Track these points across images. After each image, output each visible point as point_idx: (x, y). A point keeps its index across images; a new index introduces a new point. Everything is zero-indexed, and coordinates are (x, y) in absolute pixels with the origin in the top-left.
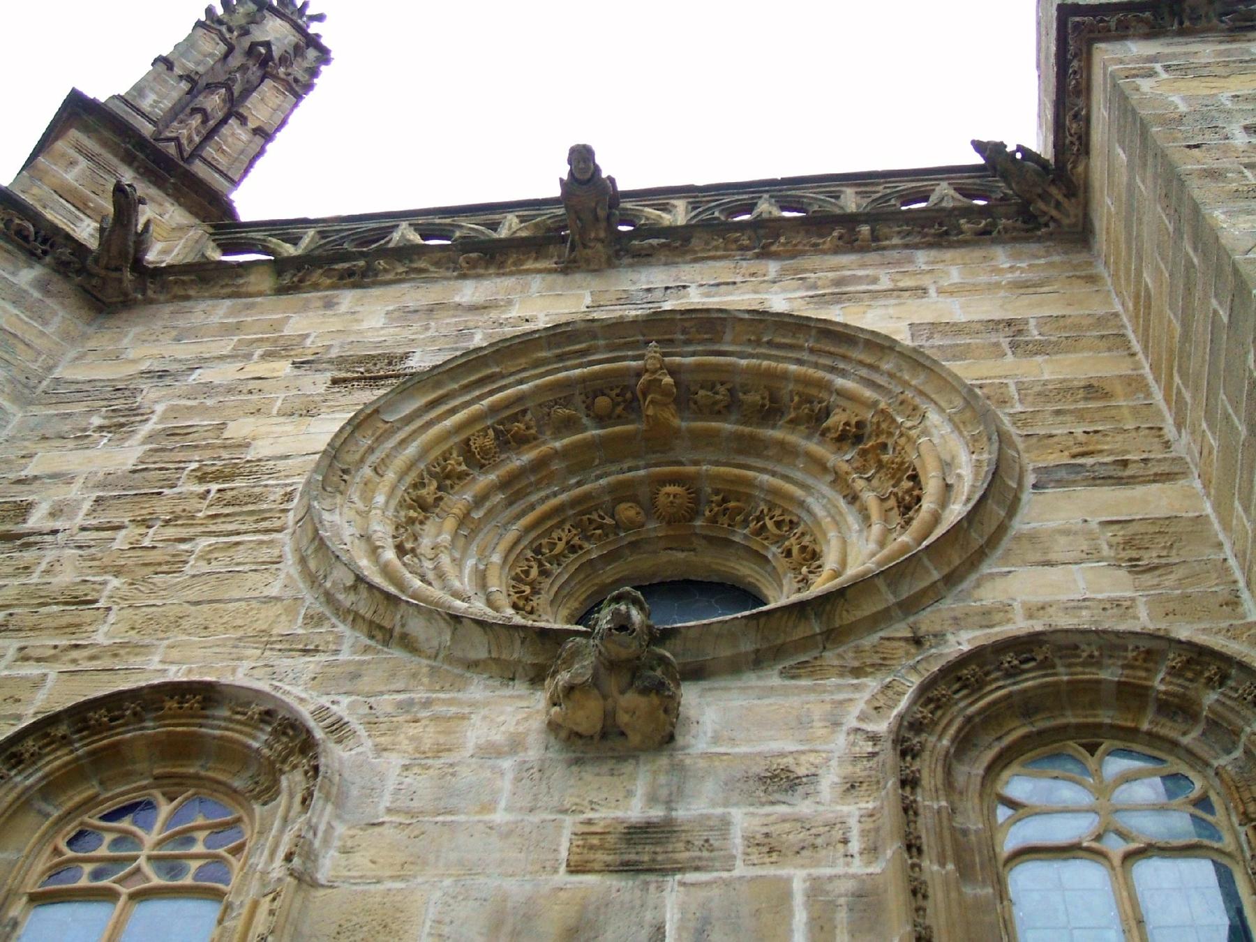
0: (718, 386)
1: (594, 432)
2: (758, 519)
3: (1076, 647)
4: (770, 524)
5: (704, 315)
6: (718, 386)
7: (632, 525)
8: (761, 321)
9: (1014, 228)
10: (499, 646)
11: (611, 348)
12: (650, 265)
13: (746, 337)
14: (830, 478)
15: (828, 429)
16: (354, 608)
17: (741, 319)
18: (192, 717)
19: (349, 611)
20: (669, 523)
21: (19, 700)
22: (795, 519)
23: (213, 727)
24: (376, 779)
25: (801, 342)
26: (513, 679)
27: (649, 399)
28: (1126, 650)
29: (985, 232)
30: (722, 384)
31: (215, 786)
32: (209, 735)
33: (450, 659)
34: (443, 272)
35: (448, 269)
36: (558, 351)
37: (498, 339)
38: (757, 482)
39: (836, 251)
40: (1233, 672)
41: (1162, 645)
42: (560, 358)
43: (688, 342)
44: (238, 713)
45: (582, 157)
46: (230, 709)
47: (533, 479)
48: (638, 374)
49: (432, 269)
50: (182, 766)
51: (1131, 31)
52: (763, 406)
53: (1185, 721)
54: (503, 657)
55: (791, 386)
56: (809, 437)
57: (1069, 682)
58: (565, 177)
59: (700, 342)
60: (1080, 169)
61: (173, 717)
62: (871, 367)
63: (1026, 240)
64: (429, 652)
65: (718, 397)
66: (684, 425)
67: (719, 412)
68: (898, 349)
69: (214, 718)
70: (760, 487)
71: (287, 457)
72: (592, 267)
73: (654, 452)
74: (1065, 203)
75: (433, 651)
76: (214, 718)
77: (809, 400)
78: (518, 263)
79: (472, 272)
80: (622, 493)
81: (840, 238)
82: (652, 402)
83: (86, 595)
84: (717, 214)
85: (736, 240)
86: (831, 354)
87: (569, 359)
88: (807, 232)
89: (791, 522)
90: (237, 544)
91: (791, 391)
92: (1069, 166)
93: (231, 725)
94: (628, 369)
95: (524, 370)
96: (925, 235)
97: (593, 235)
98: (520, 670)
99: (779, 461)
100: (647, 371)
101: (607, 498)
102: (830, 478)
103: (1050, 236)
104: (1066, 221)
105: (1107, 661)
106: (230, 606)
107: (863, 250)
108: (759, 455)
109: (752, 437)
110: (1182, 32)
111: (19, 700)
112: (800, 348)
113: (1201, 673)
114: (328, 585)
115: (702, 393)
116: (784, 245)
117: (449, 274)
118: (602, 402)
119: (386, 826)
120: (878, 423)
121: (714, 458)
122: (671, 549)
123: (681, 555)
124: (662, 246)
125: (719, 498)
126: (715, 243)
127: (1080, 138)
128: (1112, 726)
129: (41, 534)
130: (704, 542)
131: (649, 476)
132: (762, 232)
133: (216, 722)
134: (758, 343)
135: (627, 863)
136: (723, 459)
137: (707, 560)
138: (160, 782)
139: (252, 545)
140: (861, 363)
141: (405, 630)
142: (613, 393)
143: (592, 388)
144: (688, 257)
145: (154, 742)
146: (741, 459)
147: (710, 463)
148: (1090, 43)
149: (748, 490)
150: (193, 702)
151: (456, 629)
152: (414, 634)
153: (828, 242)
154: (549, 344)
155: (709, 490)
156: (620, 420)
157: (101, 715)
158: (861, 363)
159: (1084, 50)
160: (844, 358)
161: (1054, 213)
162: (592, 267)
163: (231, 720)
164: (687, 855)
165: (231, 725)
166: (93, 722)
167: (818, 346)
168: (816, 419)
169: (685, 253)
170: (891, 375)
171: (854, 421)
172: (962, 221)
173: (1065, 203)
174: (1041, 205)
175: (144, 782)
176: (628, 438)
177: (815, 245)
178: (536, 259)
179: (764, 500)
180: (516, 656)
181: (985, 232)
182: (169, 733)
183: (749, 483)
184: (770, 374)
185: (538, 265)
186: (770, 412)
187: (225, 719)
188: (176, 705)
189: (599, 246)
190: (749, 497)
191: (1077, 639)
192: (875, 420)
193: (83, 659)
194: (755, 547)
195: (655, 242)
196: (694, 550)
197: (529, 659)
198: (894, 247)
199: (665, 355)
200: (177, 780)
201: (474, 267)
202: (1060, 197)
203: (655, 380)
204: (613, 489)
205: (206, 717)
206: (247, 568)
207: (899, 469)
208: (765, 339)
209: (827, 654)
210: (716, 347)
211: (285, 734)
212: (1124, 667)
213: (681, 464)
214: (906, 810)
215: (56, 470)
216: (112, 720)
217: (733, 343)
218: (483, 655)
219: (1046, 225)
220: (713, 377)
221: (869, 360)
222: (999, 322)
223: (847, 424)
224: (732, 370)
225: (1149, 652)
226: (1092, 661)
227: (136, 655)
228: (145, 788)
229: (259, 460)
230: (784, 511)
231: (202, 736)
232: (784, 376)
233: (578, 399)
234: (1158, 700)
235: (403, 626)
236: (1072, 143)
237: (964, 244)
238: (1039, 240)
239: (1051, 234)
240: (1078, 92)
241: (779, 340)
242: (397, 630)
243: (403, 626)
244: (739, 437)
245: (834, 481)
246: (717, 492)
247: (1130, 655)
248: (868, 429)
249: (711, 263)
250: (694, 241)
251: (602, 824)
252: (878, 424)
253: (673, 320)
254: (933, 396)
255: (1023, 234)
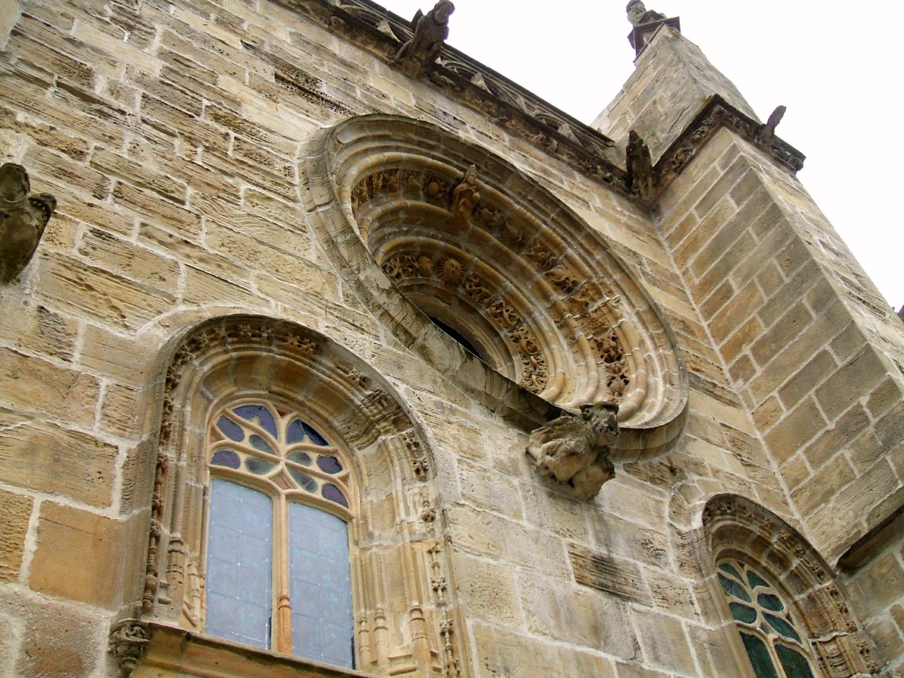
0: (496, 212)
1: (422, 203)
2: (498, 307)
3: (744, 508)
4: (506, 315)
5: (504, 164)
6: (496, 212)
7: (426, 274)
8: (531, 185)
9: (620, 187)
10: (492, 385)
11: (446, 153)
12: (438, 91)
13: (518, 190)
14: (548, 305)
15: (553, 274)
16: (385, 306)
17: (522, 178)
18: (304, 356)
19: (379, 307)
20: (446, 283)
21: (164, 280)
22: (522, 320)
23: (318, 370)
24: (447, 465)
25: (548, 211)
26: (493, 411)
27: (462, 201)
28: (763, 518)
29: (607, 180)
30: (499, 211)
31: (314, 416)
32: (318, 376)
33: (453, 378)
34: (317, 19)
35: (321, 19)
36: (421, 139)
37: (396, 113)
38: (504, 284)
39: (536, 146)
40: (808, 552)
41: (778, 522)
42: (420, 144)
43: (486, 173)
44: (339, 368)
45: (444, 9)
46: (335, 363)
47: (391, 219)
48: (459, 180)
49: (312, 13)
50: (291, 390)
51: (739, 130)
52: (518, 238)
53: (780, 568)
54: (493, 395)
55: (537, 236)
56: (539, 271)
57: (742, 527)
58: (425, 13)
59: (492, 177)
60: (670, 177)
61: (291, 350)
62: (587, 251)
63: (623, 195)
64: (440, 367)
65: (495, 219)
66: (471, 225)
67: (490, 227)
68: (608, 251)
69: (320, 364)
70: (504, 289)
71: (272, 132)
72: (408, 73)
73: (448, 232)
74: (651, 189)
75: (443, 368)
76: (320, 364)
77: (545, 250)
78: (365, 43)
79: (336, 31)
80: (427, 250)
81: (541, 139)
82: (464, 203)
83: (172, 192)
84: (455, 70)
85: (489, 107)
86: (564, 229)
87: (424, 147)
88: (525, 125)
89: (519, 320)
90: (269, 199)
91: (536, 239)
92: (664, 172)
93: (334, 376)
94: (454, 173)
95: (400, 141)
96: (580, 164)
97: (418, 55)
98: (500, 407)
99: (516, 277)
100: (466, 181)
101: (418, 250)
102: (548, 305)
103: (633, 201)
104: (644, 198)
105: (754, 521)
106: (287, 257)
107: (548, 153)
108: (505, 266)
109: (507, 255)
110: (757, 146)
111: (164, 280)
112: (547, 215)
113: (793, 546)
114: (362, 277)
115: (486, 210)
116: (513, 125)
117: (322, 23)
118: (434, 186)
119: (467, 508)
120: (587, 290)
121: (478, 254)
122: (438, 297)
123: (443, 305)
124: (451, 85)
125: (477, 281)
126: (477, 101)
127: (681, 163)
128: (750, 557)
129: (110, 108)
130: (457, 303)
131: (445, 247)
132: (502, 109)
133: (321, 367)
134: (524, 198)
135: (601, 584)
136: (483, 257)
137: (455, 314)
138: (273, 396)
139: (280, 206)
140: (581, 245)
141: (426, 343)
142: (443, 183)
143: (433, 175)
144: (460, 101)
145: (276, 365)
146: (492, 262)
147: (480, 258)
148: (722, 125)
149: (495, 286)
150: (308, 346)
151: (466, 361)
152: (432, 349)
153: (535, 138)
154: (417, 130)
155: (471, 273)
156: (437, 202)
157: (246, 329)
158: (581, 245)
159: (718, 125)
160: (572, 235)
161: (642, 191)
162: (408, 73)
163: (333, 371)
164: (632, 589)
165: (334, 376)
166: (242, 333)
167: (559, 220)
168: (546, 265)
169: (458, 97)
170: (598, 263)
171: (572, 279)
172: (599, 167)
173: (651, 189)
174: (640, 183)
175: (263, 392)
176: (440, 216)
177: (527, 135)
178: (376, 47)
179: (504, 297)
180: (501, 398)
181: (607, 180)
182: (290, 363)
183: (499, 283)
184: (528, 222)
185: (374, 51)
186: (518, 244)
187: (329, 368)
188: (296, 343)
189: (419, 64)
190: (494, 290)
191: (746, 504)
192: (586, 286)
193: (196, 257)
194: (493, 324)
195: (448, 81)
196: (450, 304)
197: (509, 404)
198: (563, 161)
199: (478, 177)
200: (285, 400)
201: (338, 28)
202: (650, 184)
203: (470, 191)
204: (424, 245)
205: (314, 360)
206: (286, 227)
207: (600, 326)
208: (529, 198)
209: (640, 462)
210: (501, 186)
211: (380, 402)
212: (761, 527)
213: (460, 247)
214: (177, 356)
215: (100, 46)
216: (253, 336)
217: (510, 189)
218: (480, 387)
219: (634, 194)
220: (495, 204)
221: (588, 247)
222: (630, 250)
223: (567, 279)
224: (506, 205)
225: (773, 525)
226: (749, 519)
227: (234, 272)
228: (260, 396)
229: (254, 124)
230: (515, 310)
231: (313, 375)
232: (537, 228)
233: (422, 177)
234: (772, 552)
235: (425, 339)
236: (674, 163)
237: (596, 180)
238: (628, 199)
239: (635, 200)
240: (696, 142)
241: (536, 202)
242: (420, 341)
243: (425, 339)
244: (498, 250)
245: (550, 308)
246: (476, 276)
247: (766, 523)
248: (578, 288)
249: (472, 113)
250: (466, 93)
251: (580, 549)
252: (587, 290)
253: (484, 155)
254: (627, 293)
255: (623, 192)
